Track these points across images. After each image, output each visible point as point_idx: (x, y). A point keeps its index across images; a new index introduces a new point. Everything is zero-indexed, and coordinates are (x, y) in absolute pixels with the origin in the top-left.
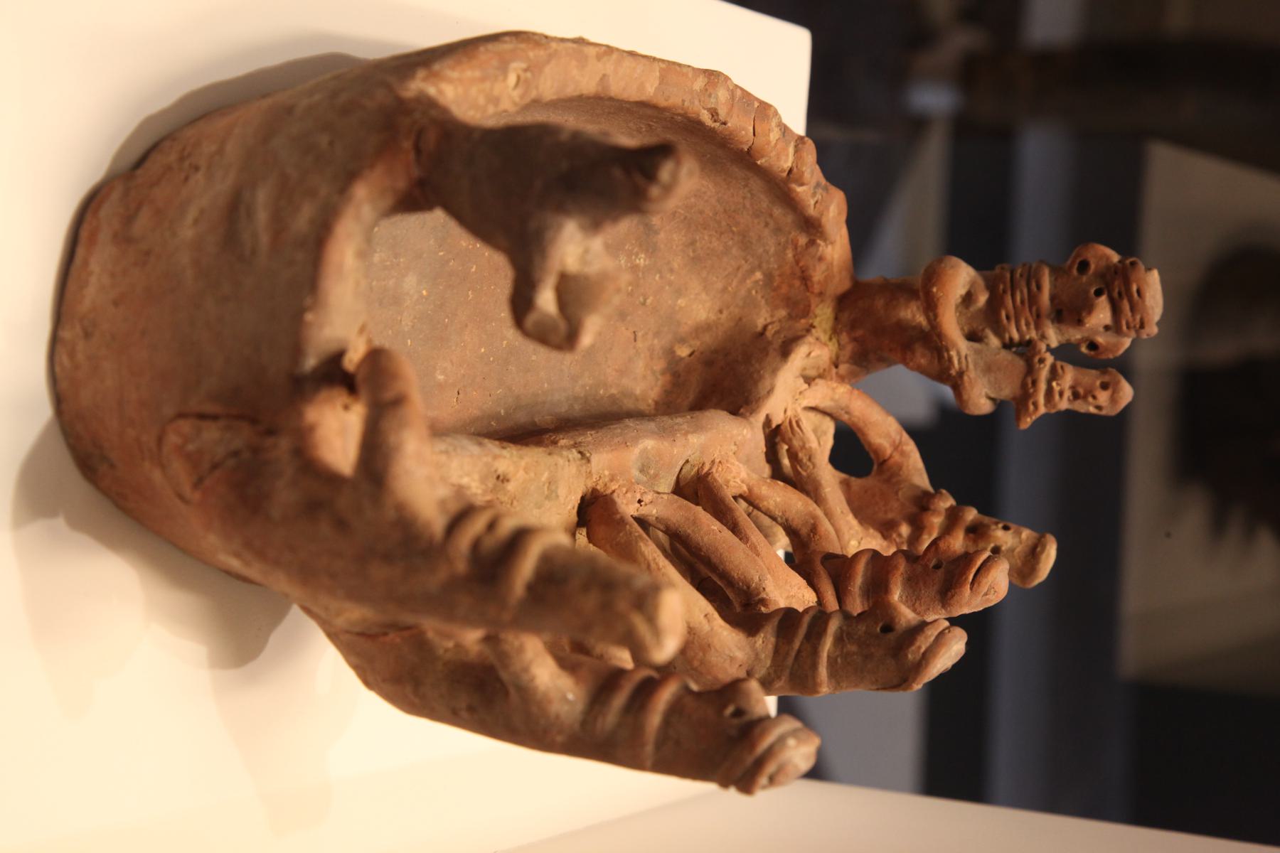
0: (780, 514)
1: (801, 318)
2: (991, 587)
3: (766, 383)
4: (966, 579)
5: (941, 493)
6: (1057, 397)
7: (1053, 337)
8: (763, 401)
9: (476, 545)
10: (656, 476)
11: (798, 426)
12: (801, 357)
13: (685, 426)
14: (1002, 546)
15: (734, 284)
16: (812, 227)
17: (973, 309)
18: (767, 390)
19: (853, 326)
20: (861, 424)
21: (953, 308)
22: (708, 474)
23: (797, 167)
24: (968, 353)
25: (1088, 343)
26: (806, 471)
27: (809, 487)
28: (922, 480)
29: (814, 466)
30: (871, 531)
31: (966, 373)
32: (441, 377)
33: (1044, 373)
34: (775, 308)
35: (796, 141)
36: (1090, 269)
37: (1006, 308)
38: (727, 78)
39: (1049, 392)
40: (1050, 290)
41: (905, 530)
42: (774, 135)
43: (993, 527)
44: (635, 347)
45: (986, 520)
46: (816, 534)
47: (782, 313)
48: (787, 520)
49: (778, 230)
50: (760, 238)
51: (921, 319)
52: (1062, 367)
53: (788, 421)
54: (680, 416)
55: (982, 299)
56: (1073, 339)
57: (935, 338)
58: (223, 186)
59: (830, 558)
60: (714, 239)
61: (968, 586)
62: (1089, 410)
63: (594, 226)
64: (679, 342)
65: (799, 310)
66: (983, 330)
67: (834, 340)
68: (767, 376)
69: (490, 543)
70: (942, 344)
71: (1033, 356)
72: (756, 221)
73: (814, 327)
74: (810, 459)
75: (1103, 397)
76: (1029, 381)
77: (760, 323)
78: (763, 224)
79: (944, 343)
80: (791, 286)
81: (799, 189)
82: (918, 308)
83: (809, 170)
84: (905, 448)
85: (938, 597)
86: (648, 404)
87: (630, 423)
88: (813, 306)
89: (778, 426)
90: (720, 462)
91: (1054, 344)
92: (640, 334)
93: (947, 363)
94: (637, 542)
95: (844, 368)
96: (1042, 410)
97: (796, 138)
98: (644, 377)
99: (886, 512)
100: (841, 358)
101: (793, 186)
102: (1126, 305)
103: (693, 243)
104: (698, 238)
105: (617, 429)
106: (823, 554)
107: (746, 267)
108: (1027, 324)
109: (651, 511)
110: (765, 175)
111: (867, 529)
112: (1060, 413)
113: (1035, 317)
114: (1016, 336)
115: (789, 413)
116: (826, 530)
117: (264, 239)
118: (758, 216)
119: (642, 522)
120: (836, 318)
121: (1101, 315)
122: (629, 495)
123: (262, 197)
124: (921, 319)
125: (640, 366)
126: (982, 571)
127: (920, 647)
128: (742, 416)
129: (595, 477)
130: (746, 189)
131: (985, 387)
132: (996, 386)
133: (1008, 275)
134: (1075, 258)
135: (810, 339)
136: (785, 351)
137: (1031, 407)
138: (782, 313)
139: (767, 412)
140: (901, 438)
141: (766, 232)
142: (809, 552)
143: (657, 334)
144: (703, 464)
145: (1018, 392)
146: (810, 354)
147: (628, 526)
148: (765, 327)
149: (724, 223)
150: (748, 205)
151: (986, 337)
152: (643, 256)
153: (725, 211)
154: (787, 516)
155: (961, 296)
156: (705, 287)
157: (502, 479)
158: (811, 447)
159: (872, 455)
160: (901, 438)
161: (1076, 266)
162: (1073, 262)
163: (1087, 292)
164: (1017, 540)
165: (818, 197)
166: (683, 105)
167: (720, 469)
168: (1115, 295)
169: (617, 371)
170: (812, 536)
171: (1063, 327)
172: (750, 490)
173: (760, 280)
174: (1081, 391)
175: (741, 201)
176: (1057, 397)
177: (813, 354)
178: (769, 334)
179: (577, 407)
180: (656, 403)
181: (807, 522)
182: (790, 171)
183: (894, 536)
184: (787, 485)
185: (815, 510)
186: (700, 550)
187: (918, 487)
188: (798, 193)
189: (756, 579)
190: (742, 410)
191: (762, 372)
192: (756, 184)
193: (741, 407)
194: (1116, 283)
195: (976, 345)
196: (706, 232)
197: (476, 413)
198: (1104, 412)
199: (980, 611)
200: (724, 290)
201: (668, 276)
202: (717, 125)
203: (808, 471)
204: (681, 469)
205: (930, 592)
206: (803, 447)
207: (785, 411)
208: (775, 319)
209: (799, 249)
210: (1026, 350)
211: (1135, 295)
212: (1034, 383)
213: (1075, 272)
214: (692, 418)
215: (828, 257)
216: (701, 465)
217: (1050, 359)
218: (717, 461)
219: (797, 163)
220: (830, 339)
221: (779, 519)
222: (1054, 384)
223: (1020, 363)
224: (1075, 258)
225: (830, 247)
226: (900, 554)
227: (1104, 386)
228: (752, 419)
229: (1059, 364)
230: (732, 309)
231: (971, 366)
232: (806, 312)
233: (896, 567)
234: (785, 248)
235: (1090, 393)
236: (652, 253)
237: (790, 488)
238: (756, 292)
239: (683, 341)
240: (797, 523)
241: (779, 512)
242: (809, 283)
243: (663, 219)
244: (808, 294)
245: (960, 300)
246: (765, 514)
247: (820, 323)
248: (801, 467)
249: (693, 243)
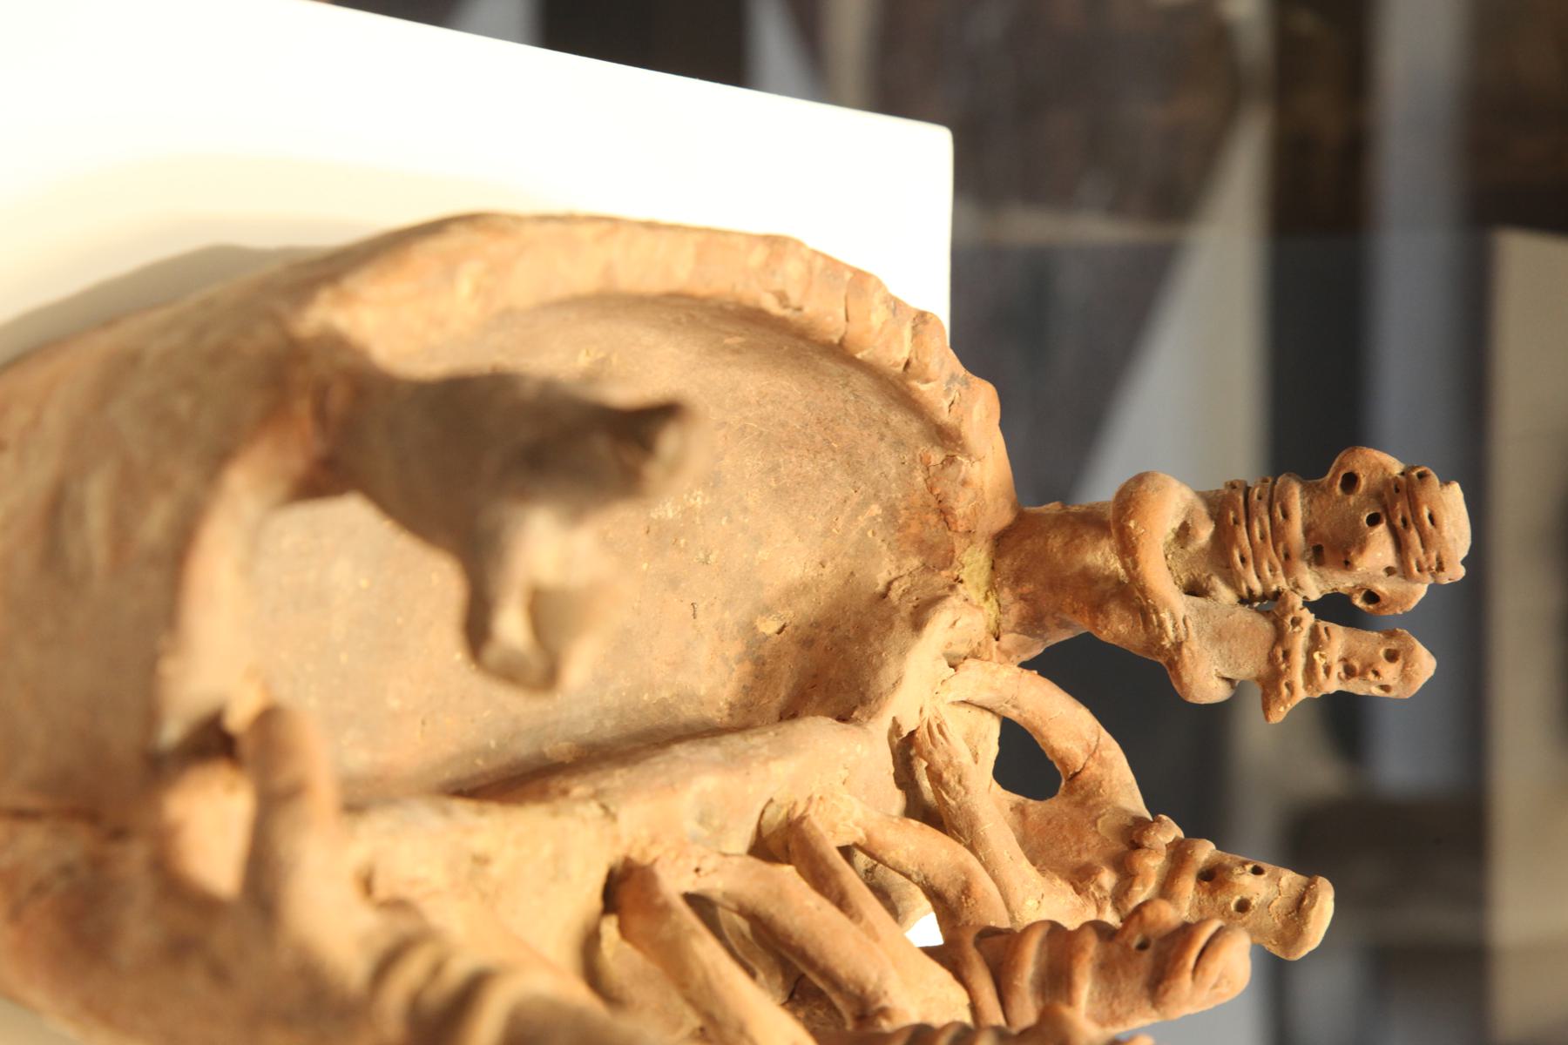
0: (916, 869)
1: (941, 569)
2: (1222, 977)
4: (1185, 965)
5: (1159, 821)
6: (1322, 675)
7: (1313, 584)
8: (887, 699)
9: (415, 1004)
10: (722, 829)
11: (941, 732)
12: (942, 629)
13: (765, 751)
14: (1252, 898)
15: (840, 523)
16: (946, 437)
17: (1192, 548)
18: (893, 681)
19: (1018, 579)
20: (1037, 722)
21: (1161, 550)
22: (802, 819)
23: (917, 358)
24: (1188, 613)
25: (1363, 592)
26: (954, 799)
27: (961, 823)
28: (1132, 800)
30: (1058, 881)
31: (1184, 645)
32: (394, 703)
33: (1300, 641)
34: (904, 554)
35: (914, 319)
36: (1359, 485)
37: (1240, 546)
38: (799, 244)
39: (1310, 667)
41: (1108, 879)
42: (878, 317)
43: (1238, 870)
44: (694, 627)
45: (1228, 859)
46: (969, 897)
47: (914, 562)
48: (926, 878)
49: (899, 444)
50: (873, 456)
51: (1115, 565)
52: (1326, 629)
53: (925, 726)
54: (758, 734)
55: (1204, 533)
56: (1341, 589)
57: (1137, 594)
58: (40, 474)
59: (988, 934)
60: (805, 461)
61: (1187, 976)
62: (1370, 692)
63: (576, 515)
64: (762, 614)
65: (938, 557)
66: (1209, 578)
67: (992, 600)
68: (891, 660)
69: (436, 996)
70: (1147, 602)
71: (1284, 615)
72: (865, 433)
73: (961, 582)
74: (960, 782)
75: (1390, 672)
77: (881, 579)
78: (876, 437)
79: (1149, 601)
80: (924, 523)
81: (923, 387)
82: (1112, 550)
83: (937, 360)
84: (1104, 754)
85: (1146, 993)
86: (717, 713)
87: (680, 750)
88: (958, 552)
89: (912, 734)
90: (821, 798)
91: (1315, 596)
92: (701, 607)
93: (1157, 630)
95: (1008, 640)
96: (1301, 694)
97: (914, 316)
98: (711, 669)
99: (1079, 853)
100: (1004, 625)
101: (914, 383)
102: (1414, 537)
103: (774, 469)
104: (781, 460)
105: (660, 762)
106: (978, 930)
107: (856, 498)
108: (1273, 569)
109: (715, 884)
110: (870, 370)
111: (1051, 880)
112: (1327, 697)
113: (1283, 558)
114: (1258, 588)
115: (926, 714)
116: (984, 890)
117: (100, 554)
118: (868, 426)
119: (699, 903)
121: (1379, 551)
122: (681, 863)
123: (96, 494)
124: (1115, 565)
125: (702, 653)
126: (1208, 952)
128: (856, 722)
129: (626, 841)
130: (848, 390)
131: (1215, 664)
132: (1232, 661)
133: (1241, 498)
134: (1338, 470)
135: (954, 600)
136: (918, 623)
137: (1285, 691)
138: (914, 562)
139: (894, 715)
140: (1098, 740)
141: (883, 447)
142: (960, 924)
143: (727, 604)
144: (795, 804)
145: (1264, 668)
146: (955, 623)
148: (889, 585)
149: (818, 438)
150: (852, 411)
151: (1214, 589)
152: (700, 493)
153: (819, 421)
154: (926, 872)
155: (1173, 530)
156: (797, 531)
157: (481, 861)
158: (960, 764)
159: (1058, 767)
160: (1098, 740)
161: (1339, 482)
162: (1335, 476)
163: (1357, 520)
165: (954, 395)
167: (821, 809)
168: (1399, 523)
169: (668, 664)
170: (963, 900)
171: (1325, 571)
172: (868, 836)
173: (877, 515)
174: (1357, 665)
175: (841, 405)
176: (1322, 675)
177: (959, 624)
178: (894, 595)
179: (609, 723)
180: (732, 706)
181: (956, 880)
182: (907, 364)
183: (1092, 888)
184: (925, 826)
185: (966, 860)
186: (790, 937)
187: (1126, 811)
188: (922, 393)
190: (856, 714)
191: (884, 655)
192: (860, 381)
193: (855, 708)
194: (1399, 506)
195: (1199, 601)
196: (792, 451)
197: (452, 749)
198: (1393, 694)
199: (1210, 1011)
200: (827, 532)
201: (741, 518)
202: (787, 313)
203: (958, 800)
204: (763, 813)
205: (1133, 985)
206: (949, 763)
207: (921, 711)
209: (932, 470)
210: (1271, 605)
211: (1428, 522)
212: (1286, 655)
213: (1338, 490)
214: (777, 734)
215: (976, 480)
216: (791, 806)
217: (1308, 618)
218: (817, 796)
219: (917, 353)
220: (986, 598)
221: (914, 877)
222: (1316, 656)
223: (1265, 626)
224: (1338, 470)
225: (977, 465)
226: (1089, 929)
227: (1392, 656)
228: (870, 727)
229: (1322, 624)
230: (839, 559)
231: (1193, 633)
232: (948, 561)
233: (1083, 949)
234: (912, 470)
235: (1370, 668)
236: (713, 487)
237: (929, 829)
238: (874, 533)
239: (767, 610)
240: (940, 881)
241: (914, 866)
242: (949, 517)
243: (726, 438)
244: (950, 534)
245: (1172, 536)
246: (894, 869)
247: (970, 575)
248: (947, 793)
249: (774, 469)
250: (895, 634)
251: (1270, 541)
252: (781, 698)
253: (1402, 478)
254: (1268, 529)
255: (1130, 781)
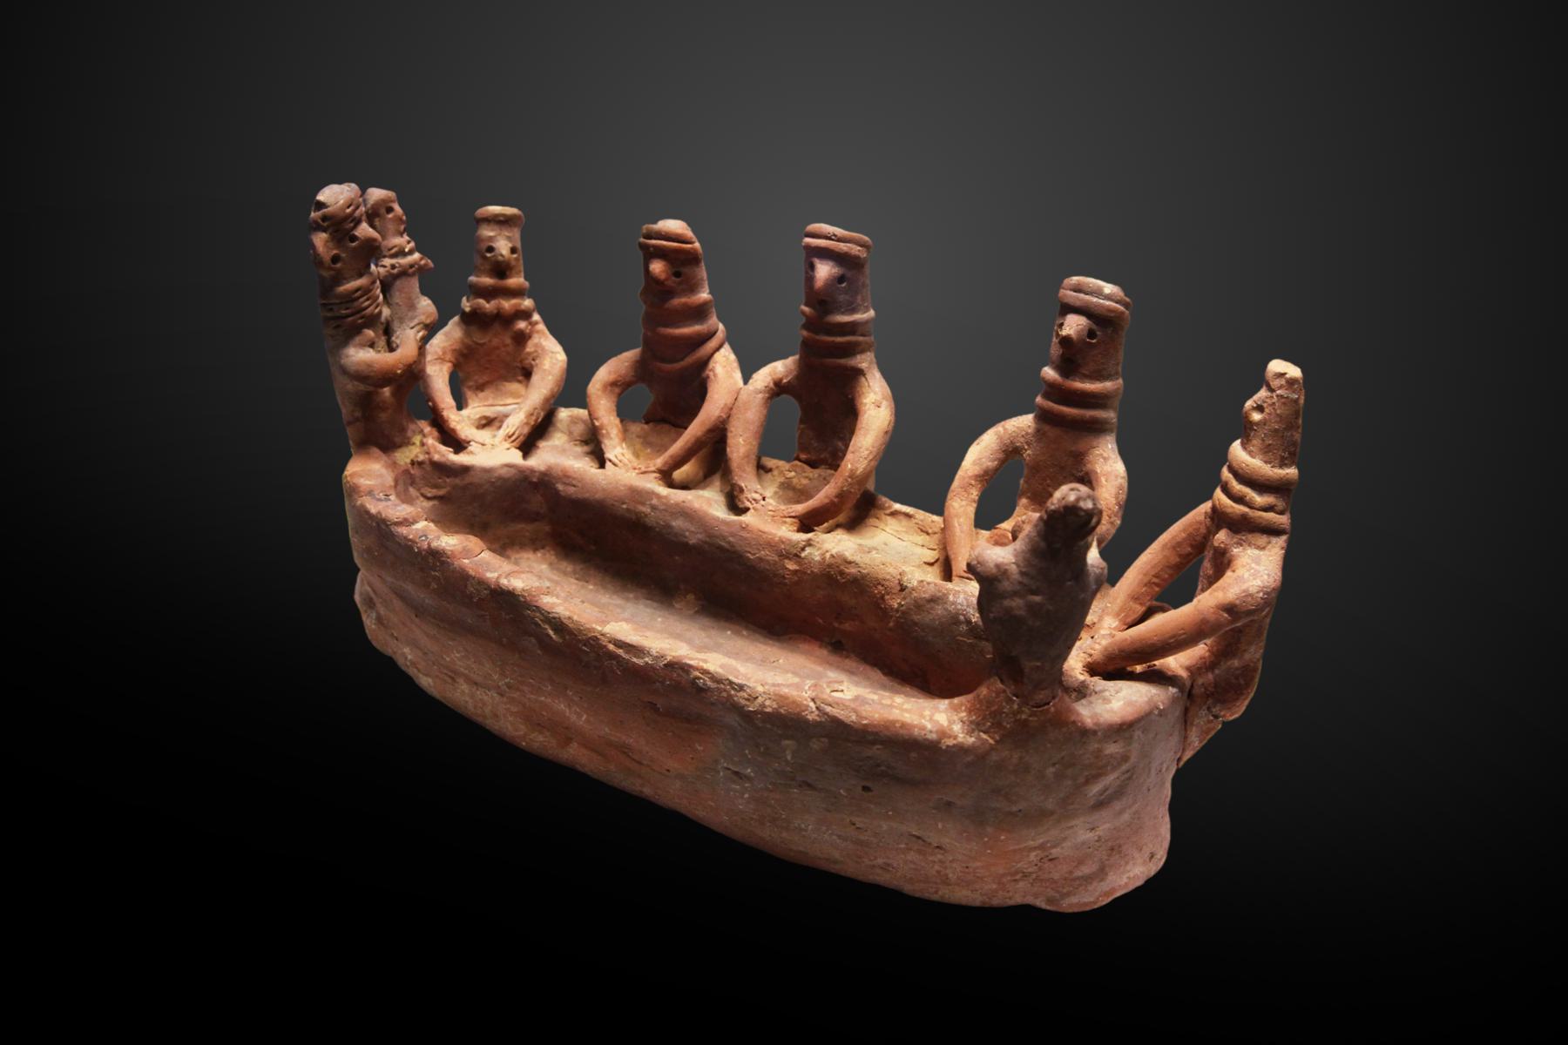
3: (504, 472)
11: (513, 434)
18: (509, 469)
29: (535, 409)
40: (355, 280)
68: (496, 475)
74: (532, 414)
76: (411, 271)
94: (857, 477)
96: (417, 256)
99: (505, 346)
120: (400, 446)
127: (859, 251)
147: (845, 489)
148: (429, 499)
158: (526, 417)
163: (355, 248)
164: (499, 238)
166: (803, 549)
189: (760, 396)
206: (527, 424)
207: (508, 449)
208: (418, 495)
222: (407, 250)
231: (416, 321)
247: (408, 457)
250: (476, 480)
251: (369, 295)
252: (523, 526)
253: (330, 230)
254: (365, 298)
255: (443, 337)
